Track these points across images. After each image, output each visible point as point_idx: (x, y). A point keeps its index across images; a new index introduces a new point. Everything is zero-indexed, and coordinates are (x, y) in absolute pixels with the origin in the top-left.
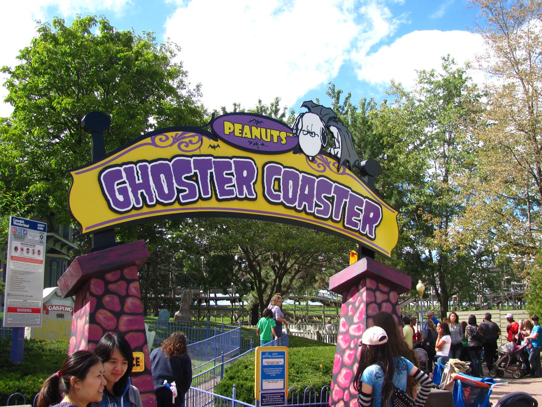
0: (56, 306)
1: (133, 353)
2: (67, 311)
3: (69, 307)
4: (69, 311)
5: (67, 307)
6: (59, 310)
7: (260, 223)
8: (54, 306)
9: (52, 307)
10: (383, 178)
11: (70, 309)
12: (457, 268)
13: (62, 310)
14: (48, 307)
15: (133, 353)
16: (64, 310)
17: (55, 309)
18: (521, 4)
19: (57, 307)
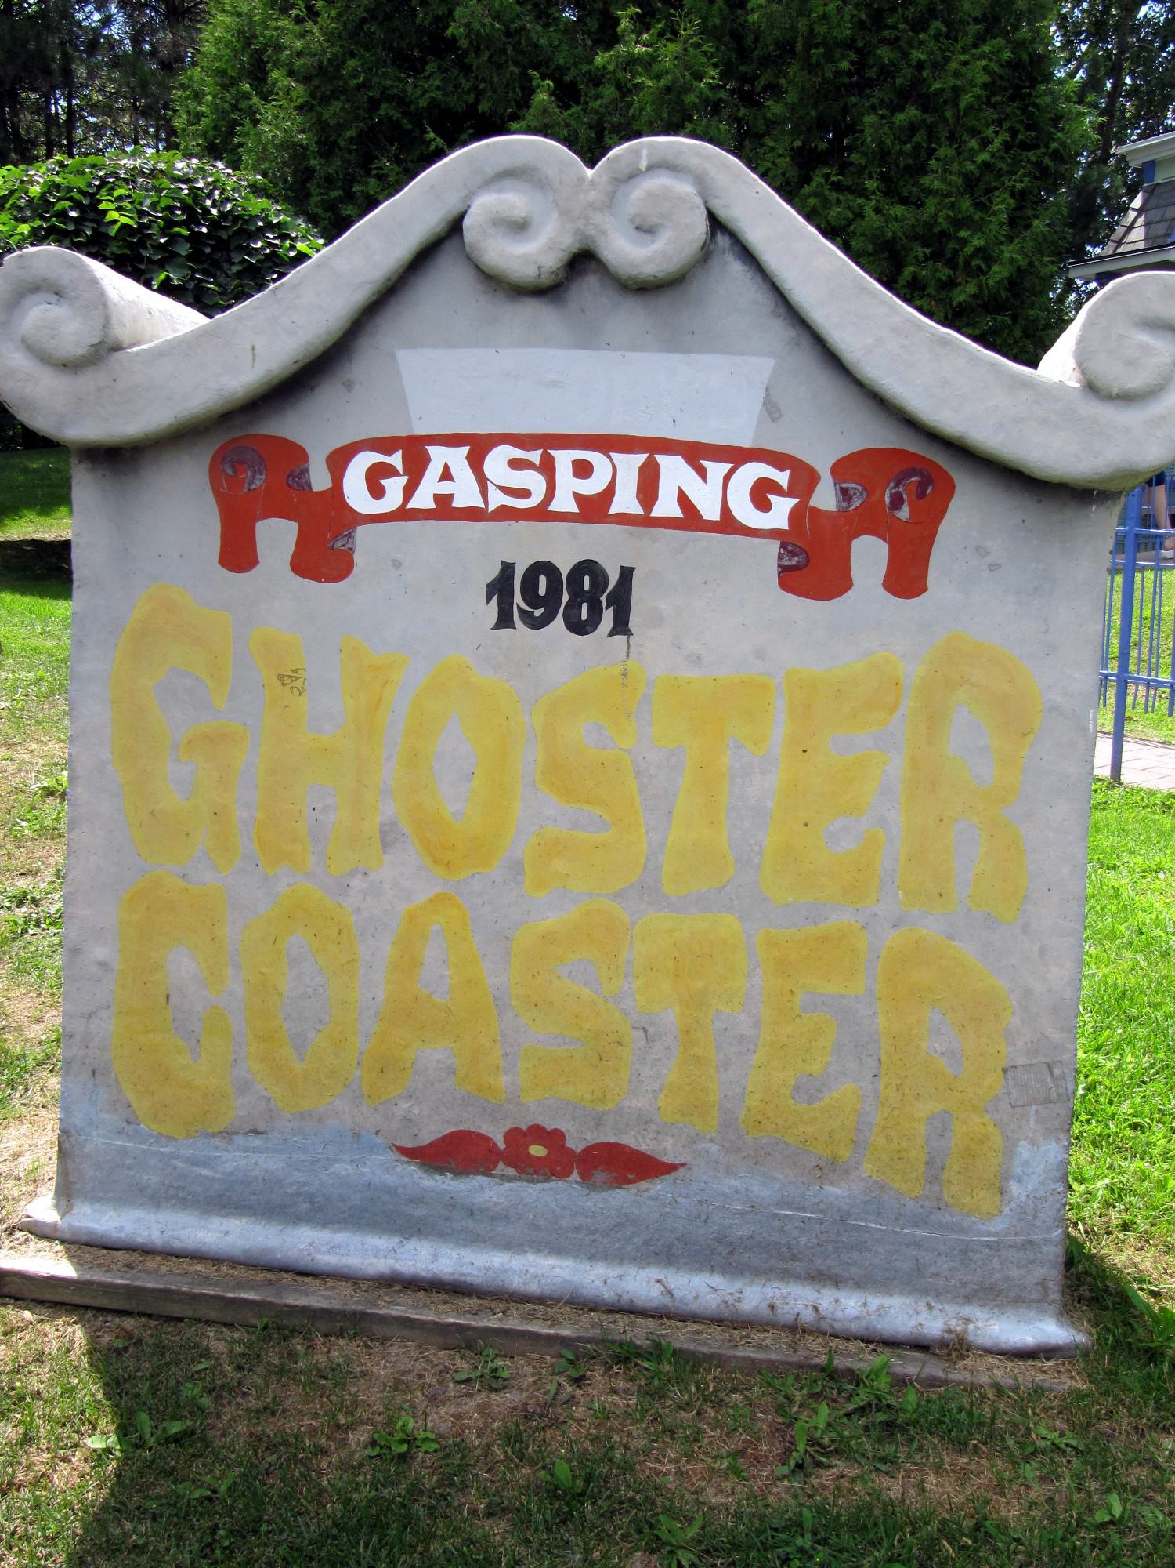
0: (478, 447)
1: (787, 528)
2: (690, 517)
3: (737, 456)
4: (728, 524)
5: (696, 454)
6: (541, 513)
7: (290, 1276)
8: (439, 455)
9: (416, 468)
10: (676, 1461)
11: (761, 495)
12: (18, 1059)
13: (594, 509)
14: (339, 461)
15: (787, 528)
16: (625, 501)
17: (466, 495)
18: (40, 900)
19: (497, 462)
